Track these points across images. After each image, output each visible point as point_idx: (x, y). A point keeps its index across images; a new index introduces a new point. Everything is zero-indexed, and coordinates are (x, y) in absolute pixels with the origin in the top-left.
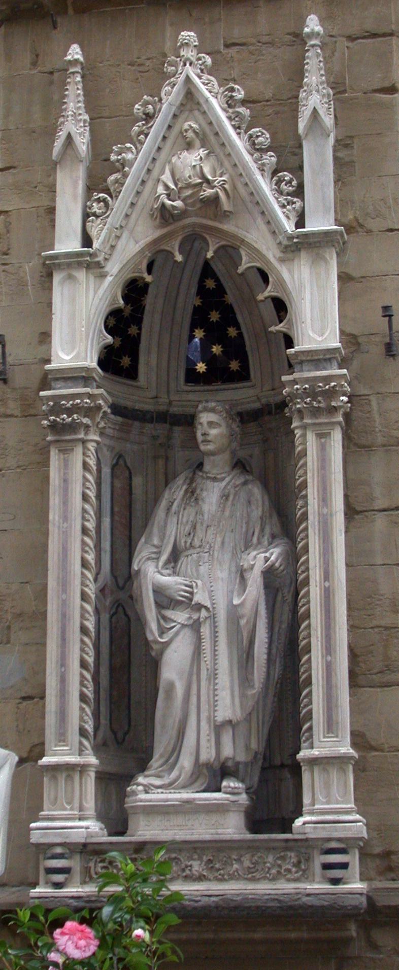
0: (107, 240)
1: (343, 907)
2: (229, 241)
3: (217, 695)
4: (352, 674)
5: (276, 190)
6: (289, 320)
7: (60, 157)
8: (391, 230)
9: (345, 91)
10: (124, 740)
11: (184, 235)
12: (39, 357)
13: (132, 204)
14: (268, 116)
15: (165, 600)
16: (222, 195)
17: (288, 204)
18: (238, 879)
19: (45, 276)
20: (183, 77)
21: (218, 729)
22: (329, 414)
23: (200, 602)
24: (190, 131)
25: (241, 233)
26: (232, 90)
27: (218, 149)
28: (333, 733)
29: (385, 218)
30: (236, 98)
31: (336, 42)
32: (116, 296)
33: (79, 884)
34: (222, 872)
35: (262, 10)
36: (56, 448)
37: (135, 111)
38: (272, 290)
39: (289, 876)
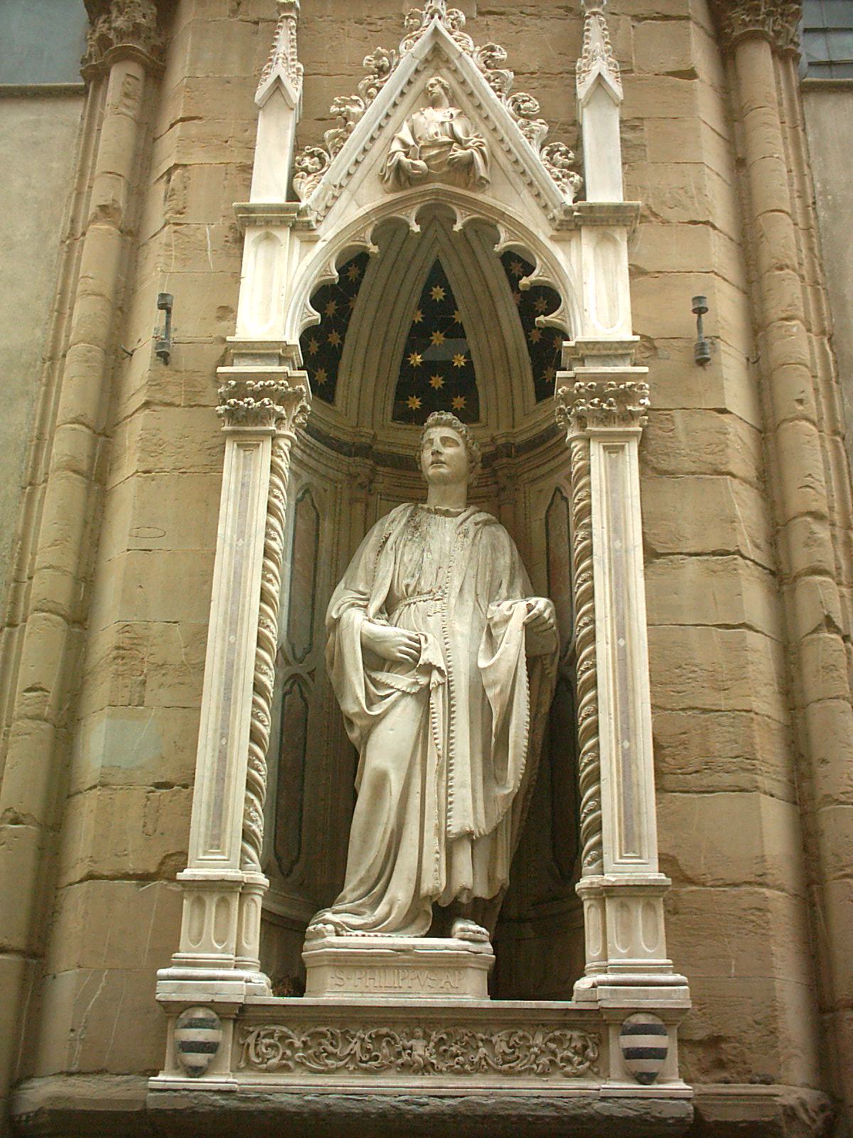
0: (322, 196)
2: (483, 214)
3: (451, 795)
4: (659, 773)
8: (695, 223)
9: (631, 71)
10: (291, 871)
11: (422, 205)
12: (214, 336)
13: (357, 162)
15: (376, 659)
16: (478, 157)
17: (563, 177)
18: (486, 1072)
20: (431, 28)
21: (451, 846)
23: (431, 661)
24: (438, 86)
25: (500, 205)
26: (492, 49)
27: (472, 112)
28: (634, 852)
29: (686, 209)
31: (619, 20)
33: (228, 1072)
37: (365, 62)
38: (541, 274)
39: (568, 1069)
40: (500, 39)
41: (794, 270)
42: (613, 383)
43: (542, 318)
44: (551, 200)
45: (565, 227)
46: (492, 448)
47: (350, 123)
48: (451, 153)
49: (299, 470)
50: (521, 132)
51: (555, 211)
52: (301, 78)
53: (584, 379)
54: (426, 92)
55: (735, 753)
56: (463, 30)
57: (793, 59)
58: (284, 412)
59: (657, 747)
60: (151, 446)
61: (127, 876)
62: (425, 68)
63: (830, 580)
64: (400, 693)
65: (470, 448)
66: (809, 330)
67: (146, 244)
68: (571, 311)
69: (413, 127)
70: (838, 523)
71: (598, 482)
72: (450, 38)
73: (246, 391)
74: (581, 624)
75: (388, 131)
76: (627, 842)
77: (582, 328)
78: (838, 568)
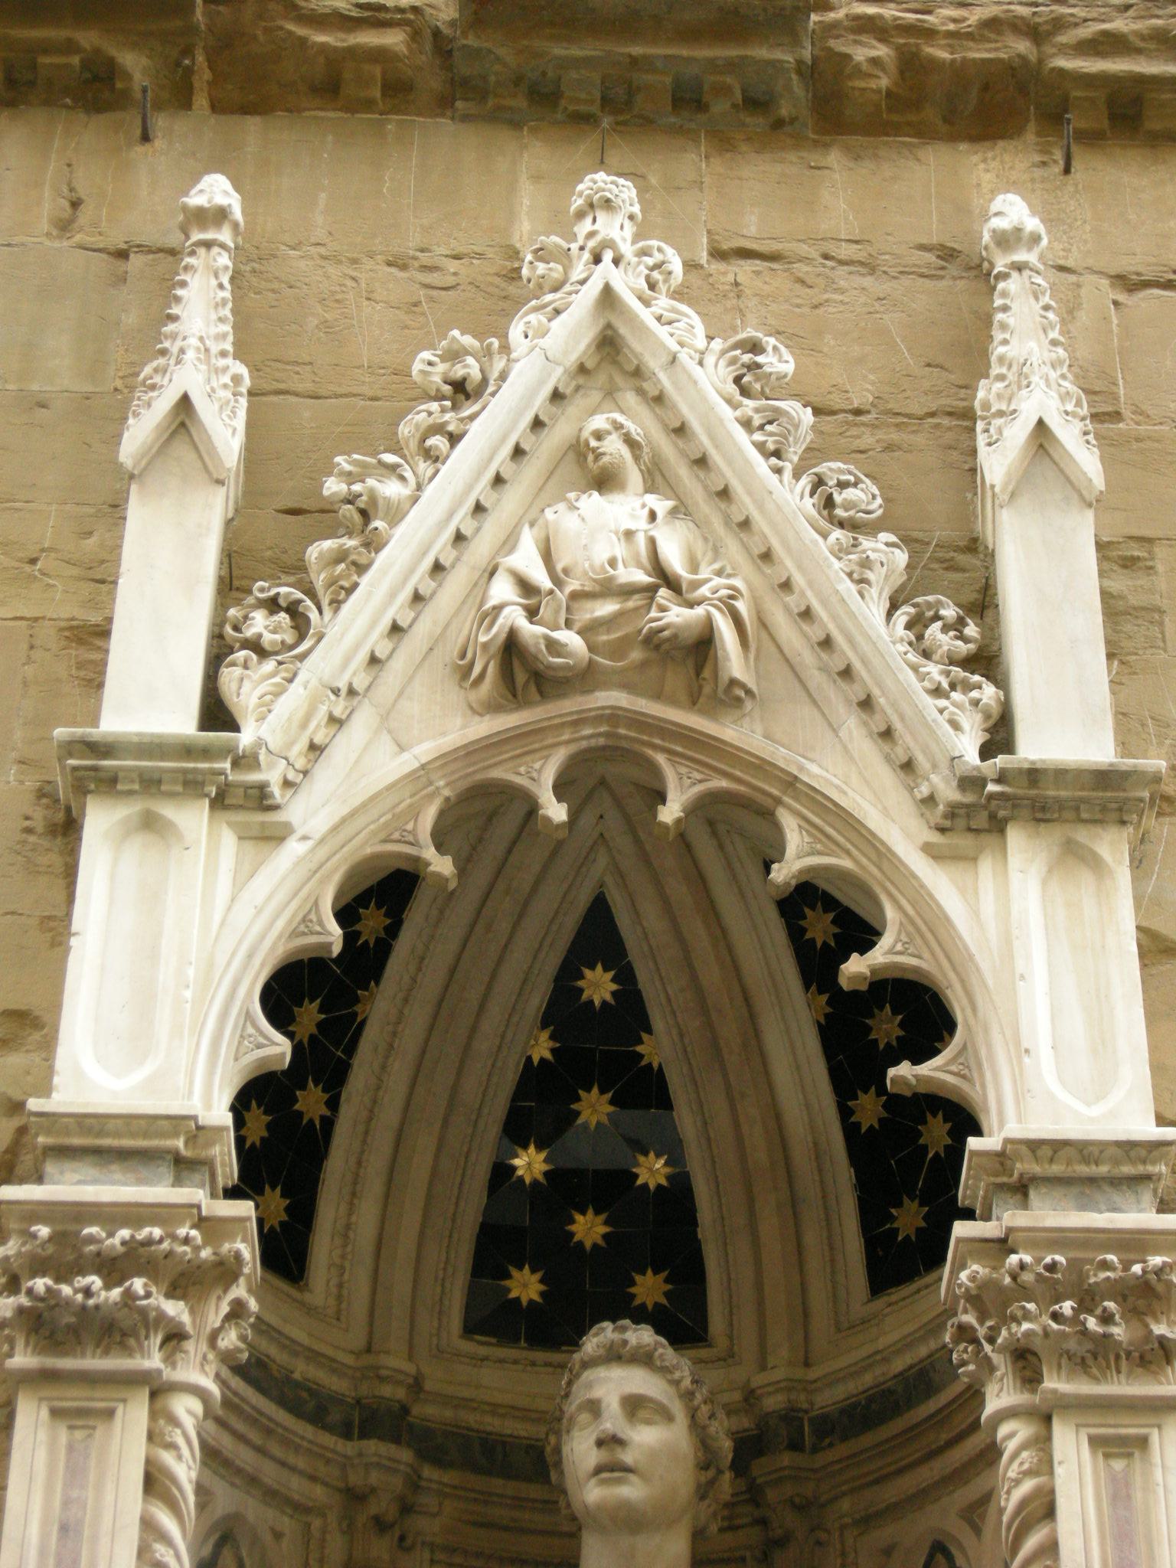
2: (739, 781)
5: (910, 644)
6: (964, 1048)
7: (144, 463)
9: (1116, 416)
11: (573, 748)
14: (861, 452)
17: (953, 686)
19: (40, 829)
20: (593, 289)
22: (1140, 1370)
25: (781, 756)
26: (755, 347)
30: (767, 369)
31: (1079, 286)
35: (837, 176)
36: (41, 1399)
38: (899, 947)
40: (771, 321)
42: (1112, 1257)
43: (903, 1070)
44: (926, 750)
45: (961, 823)
47: (377, 524)
48: (653, 614)
50: (837, 565)
51: (935, 778)
52: (243, 402)
54: (580, 451)
56: (678, 295)
58: (186, 1318)
62: (578, 388)
65: (704, 1428)
68: (983, 1053)
69: (548, 540)
71: (1079, 1543)
72: (646, 315)
73: (81, 1256)
75: (481, 549)
77: (1017, 1101)
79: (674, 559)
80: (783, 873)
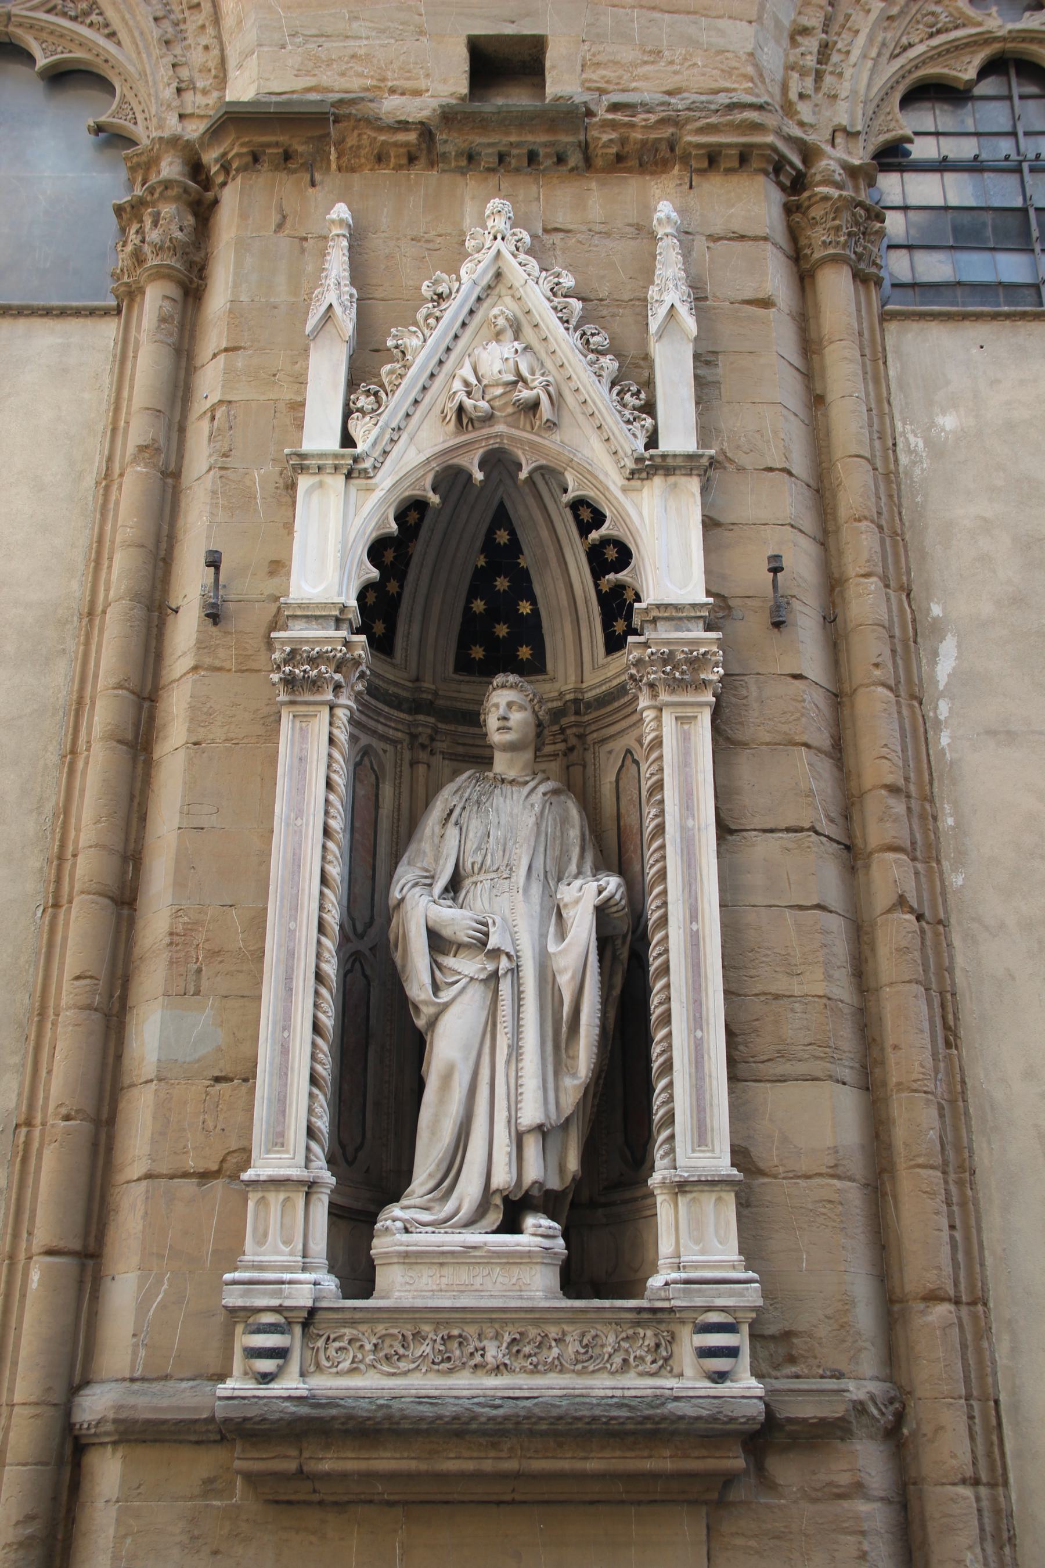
1: (732, 1420)
4: (732, 1062)
8: (770, 469)
10: (355, 1158)
11: (485, 449)
12: (266, 593)
17: (634, 419)
20: (493, 252)
32: (387, 518)
34: (534, 1359)
41: (872, 521)
46: (560, 704)
49: (356, 732)
52: (355, 305)
53: (656, 644)
55: (807, 1041)
56: (527, 252)
57: (875, 284)
58: (342, 680)
59: (730, 1033)
60: (199, 714)
61: (185, 1175)
62: (488, 295)
63: (905, 857)
64: (468, 979)
66: (887, 586)
67: (190, 488)
70: (914, 794)
74: (651, 862)
76: (699, 1136)
78: (913, 843)
79: (525, 372)
80: (571, 495)
